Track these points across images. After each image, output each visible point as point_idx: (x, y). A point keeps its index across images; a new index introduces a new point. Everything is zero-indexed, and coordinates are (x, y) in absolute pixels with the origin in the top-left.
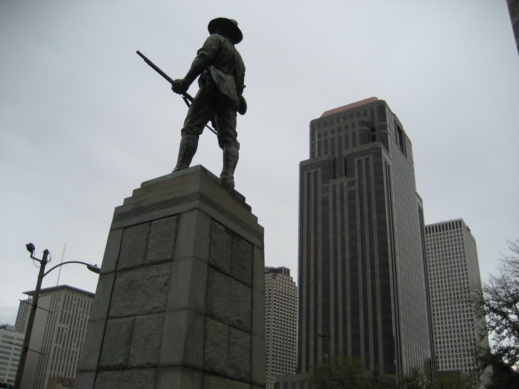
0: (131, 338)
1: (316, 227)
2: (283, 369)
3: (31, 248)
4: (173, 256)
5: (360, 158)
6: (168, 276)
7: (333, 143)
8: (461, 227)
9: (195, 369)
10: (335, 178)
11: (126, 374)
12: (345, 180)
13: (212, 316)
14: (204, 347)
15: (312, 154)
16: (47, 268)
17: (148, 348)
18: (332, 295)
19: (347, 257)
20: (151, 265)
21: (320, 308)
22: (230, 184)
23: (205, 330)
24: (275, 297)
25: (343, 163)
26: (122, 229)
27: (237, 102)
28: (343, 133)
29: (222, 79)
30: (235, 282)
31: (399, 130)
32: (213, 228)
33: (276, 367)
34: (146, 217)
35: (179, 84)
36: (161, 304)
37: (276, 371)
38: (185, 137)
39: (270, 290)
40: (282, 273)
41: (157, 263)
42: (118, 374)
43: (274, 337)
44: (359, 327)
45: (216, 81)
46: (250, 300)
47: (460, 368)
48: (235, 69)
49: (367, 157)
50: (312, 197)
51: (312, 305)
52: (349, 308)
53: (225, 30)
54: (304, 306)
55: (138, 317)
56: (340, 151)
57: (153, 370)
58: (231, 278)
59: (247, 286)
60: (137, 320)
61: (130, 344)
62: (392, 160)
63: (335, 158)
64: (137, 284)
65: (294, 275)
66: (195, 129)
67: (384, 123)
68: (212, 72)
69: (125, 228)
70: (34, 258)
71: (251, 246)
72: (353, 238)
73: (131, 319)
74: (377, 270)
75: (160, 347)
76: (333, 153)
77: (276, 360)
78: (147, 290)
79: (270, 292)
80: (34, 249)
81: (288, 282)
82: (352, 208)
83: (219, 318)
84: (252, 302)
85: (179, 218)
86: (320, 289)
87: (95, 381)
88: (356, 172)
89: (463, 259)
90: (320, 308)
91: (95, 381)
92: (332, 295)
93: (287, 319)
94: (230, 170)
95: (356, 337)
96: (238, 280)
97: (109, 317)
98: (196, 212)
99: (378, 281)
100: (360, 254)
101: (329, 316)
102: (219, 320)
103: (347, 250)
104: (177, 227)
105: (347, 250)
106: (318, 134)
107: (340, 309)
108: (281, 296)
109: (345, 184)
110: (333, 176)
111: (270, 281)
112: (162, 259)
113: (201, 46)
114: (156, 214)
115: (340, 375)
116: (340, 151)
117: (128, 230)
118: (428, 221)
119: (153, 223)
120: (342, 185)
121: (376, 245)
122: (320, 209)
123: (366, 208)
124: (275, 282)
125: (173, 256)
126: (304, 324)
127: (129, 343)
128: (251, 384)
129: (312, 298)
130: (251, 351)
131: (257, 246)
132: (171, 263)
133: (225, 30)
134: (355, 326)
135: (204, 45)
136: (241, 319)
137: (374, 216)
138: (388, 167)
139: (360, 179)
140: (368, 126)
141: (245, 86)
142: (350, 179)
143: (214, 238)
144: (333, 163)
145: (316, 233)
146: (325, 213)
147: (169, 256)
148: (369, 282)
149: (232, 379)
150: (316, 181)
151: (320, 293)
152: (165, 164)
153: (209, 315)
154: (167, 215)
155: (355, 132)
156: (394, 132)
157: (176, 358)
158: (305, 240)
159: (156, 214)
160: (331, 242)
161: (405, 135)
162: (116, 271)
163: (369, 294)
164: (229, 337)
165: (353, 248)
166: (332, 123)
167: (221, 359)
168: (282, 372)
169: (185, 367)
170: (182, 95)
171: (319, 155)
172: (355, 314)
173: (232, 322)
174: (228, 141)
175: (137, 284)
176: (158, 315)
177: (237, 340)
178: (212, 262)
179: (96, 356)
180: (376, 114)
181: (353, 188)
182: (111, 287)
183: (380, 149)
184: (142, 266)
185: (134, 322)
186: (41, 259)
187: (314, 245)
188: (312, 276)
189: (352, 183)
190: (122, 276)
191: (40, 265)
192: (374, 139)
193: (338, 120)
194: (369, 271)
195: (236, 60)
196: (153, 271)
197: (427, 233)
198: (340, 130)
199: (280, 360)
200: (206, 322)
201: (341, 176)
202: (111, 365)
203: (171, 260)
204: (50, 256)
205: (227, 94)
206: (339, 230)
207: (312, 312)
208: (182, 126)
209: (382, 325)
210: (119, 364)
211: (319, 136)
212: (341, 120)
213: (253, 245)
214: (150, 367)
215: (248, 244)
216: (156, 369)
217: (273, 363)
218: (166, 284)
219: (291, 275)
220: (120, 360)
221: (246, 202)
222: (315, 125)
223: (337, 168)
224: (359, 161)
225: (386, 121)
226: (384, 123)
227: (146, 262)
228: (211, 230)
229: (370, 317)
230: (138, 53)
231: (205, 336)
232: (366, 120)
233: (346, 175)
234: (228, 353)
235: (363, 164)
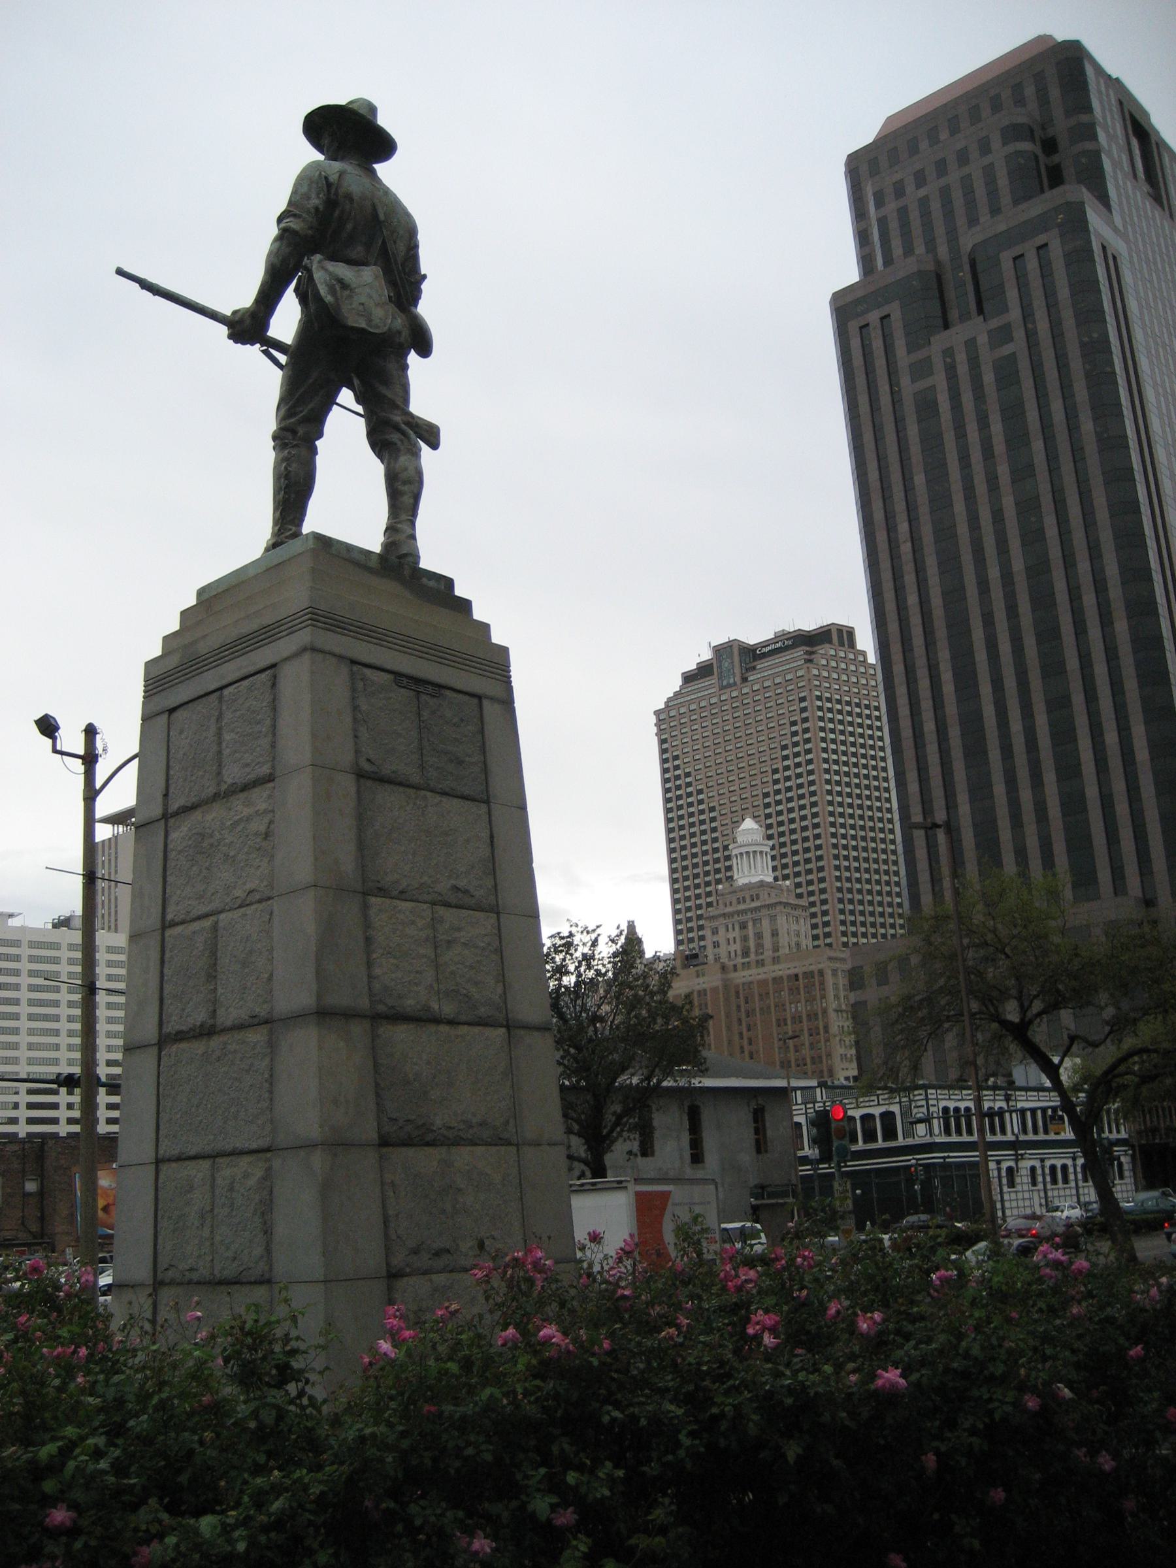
0: (215, 964)
1: (908, 488)
2: (873, 925)
3: (47, 727)
4: (273, 767)
5: (1017, 251)
6: (270, 816)
7: (926, 214)
9: (349, 1015)
10: (946, 326)
11: (215, 1042)
12: (977, 329)
13: (382, 892)
14: (369, 964)
15: (866, 262)
16: (102, 771)
17: (249, 984)
18: (986, 689)
19: (1018, 566)
20: (234, 792)
21: (954, 732)
22: (405, 555)
23: (367, 925)
24: (821, 719)
25: (965, 274)
26: (166, 716)
27: (399, 333)
28: (954, 176)
29: (344, 285)
30: (438, 798)
31: (1140, 130)
32: (360, 685)
33: (853, 923)
34: (210, 680)
35: (241, 321)
36: (262, 881)
37: (855, 935)
38: (281, 456)
39: (803, 699)
40: (830, 642)
41: (245, 788)
42: (198, 1047)
43: (834, 835)
45: (329, 299)
46: (485, 834)
48: (384, 242)
49: (1040, 239)
51: (929, 727)
52: (1041, 720)
53: (348, 133)
54: (907, 732)
55: (222, 916)
56: (952, 236)
57: (264, 1030)
58: (423, 793)
59: (474, 800)
60: (221, 924)
61: (215, 977)
62: (1124, 236)
63: (938, 263)
64: (212, 840)
65: (866, 641)
66: (301, 431)
67: (1084, 118)
68: (318, 275)
69: (172, 711)
70: (62, 753)
71: (475, 701)
72: (1028, 507)
73: (207, 923)
74: (1115, 592)
75: (270, 979)
77: (851, 901)
78: (232, 854)
79: (803, 705)
80: (57, 728)
81: (853, 668)
82: (1013, 413)
83: (402, 892)
84: (492, 837)
85: (275, 677)
86: (947, 676)
87: (159, 1066)
88: (1012, 294)
90: (954, 732)
91: (159, 1066)
92: (986, 689)
93: (866, 777)
94: (404, 517)
95: (1073, 804)
96: (444, 794)
97: (167, 924)
98: (307, 656)
99: (1121, 626)
100: (1055, 553)
102: (403, 895)
103: (1015, 544)
104: (274, 700)
105: (1015, 544)
106: (874, 194)
107: (1016, 726)
108: (840, 712)
109: (983, 339)
110: (940, 322)
111: (800, 673)
112: (252, 777)
113: (282, 206)
114: (231, 670)
115: (994, 931)
116: (952, 236)
117: (179, 715)
119: (226, 692)
120: (971, 344)
121: (1102, 515)
122: (913, 430)
123: (1057, 407)
124: (815, 672)
125: (273, 767)
126: (913, 787)
127: (212, 975)
128: (508, 1027)
129: (926, 705)
130: (500, 951)
131: (491, 699)
132: (271, 785)
133: (348, 133)
134: (1069, 771)
135: (290, 203)
136: (462, 883)
137: (1087, 426)
139: (1027, 315)
140: (1032, 138)
141: (424, 277)
142: (994, 323)
143: (364, 707)
144: (936, 282)
146: (932, 441)
147: (265, 770)
148: (1094, 633)
149: (452, 1022)
150: (888, 349)
151: (948, 689)
152: (240, 533)
153: (370, 888)
154: (252, 669)
156: (1122, 141)
157: (305, 999)
158: (881, 537)
159: (231, 670)
160: (963, 530)
161: (1162, 144)
162: (165, 816)
163: (1100, 670)
164: (434, 929)
165: (1033, 537)
166: (914, 150)
167: (416, 984)
168: (874, 936)
169: (323, 1014)
170: (258, 345)
171: (888, 261)
172: (1063, 735)
173: (440, 894)
174: (399, 437)
175: (212, 840)
176: (261, 906)
177: (457, 934)
178: (367, 767)
179: (153, 1010)
180: (1055, 93)
181: (1007, 350)
182: (161, 855)
183: (1079, 208)
184: (216, 797)
185: (215, 928)
186: (81, 752)
187: (909, 544)
188: (918, 641)
189: (1003, 335)
190: (179, 827)
191: (82, 769)
192: (1056, 178)
193: (933, 136)
194: (1089, 599)
195: (382, 217)
196: (240, 807)
198: (941, 167)
199: (871, 903)
200: (365, 907)
201: (964, 317)
202: (184, 1028)
203: (270, 778)
204: (103, 740)
205: (363, 325)
206: (981, 487)
207: (932, 750)
208: (272, 426)
210: (198, 1024)
211: (879, 204)
212: (944, 135)
213: (480, 698)
214: (259, 1024)
215: (466, 698)
216: (269, 1026)
217: (842, 912)
218: (267, 835)
219: (860, 645)
220: (199, 1016)
221: (458, 592)
222: (863, 169)
223: (951, 294)
224: (1015, 259)
225: (1089, 109)
226: (1084, 118)
227: (224, 787)
228: (354, 690)
229: (1111, 738)
230: (120, 272)
231: (368, 940)
232: (1021, 120)
233: (980, 311)
234: (437, 967)
235: (1032, 264)
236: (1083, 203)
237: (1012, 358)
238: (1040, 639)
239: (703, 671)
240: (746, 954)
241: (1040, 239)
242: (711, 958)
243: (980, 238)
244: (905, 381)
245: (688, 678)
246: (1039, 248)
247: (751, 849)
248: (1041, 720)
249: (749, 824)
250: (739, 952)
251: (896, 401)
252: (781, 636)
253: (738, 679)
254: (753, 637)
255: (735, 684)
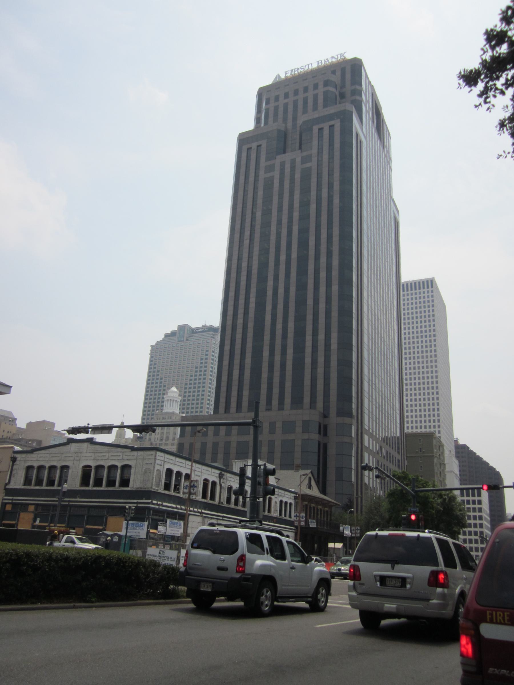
5: (321, 126)
8: (432, 287)
10: (284, 152)
12: (298, 156)
19: (294, 255)
44: (304, 352)
47: (432, 430)
49: (331, 123)
50: (252, 179)
52: (291, 325)
56: (295, 119)
76: (285, 120)
89: (433, 343)
100: (312, 252)
101: (293, 382)
107: (279, 326)
109: (298, 160)
116: (295, 119)
118: (406, 277)
120: (293, 162)
129: (241, 311)
138: (360, 143)
142: (305, 154)
145: (252, 226)
148: (323, 289)
155: (297, 100)
163: (322, 306)
171: (266, 123)
181: (308, 165)
189: (305, 160)
197: (403, 291)
207: (239, 331)
209: (338, 349)
211: (267, 103)
225: (361, 85)
229: (321, 337)
233: (300, 148)
235: (326, 132)
236: (352, 112)
237: (310, 169)
238: (298, 289)
239: (173, 334)
240: (162, 440)
241: (331, 123)
242: (147, 439)
243: (306, 119)
244: (262, 173)
245: (167, 336)
246: (330, 126)
247: (172, 399)
248: (291, 325)
249: (174, 389)
250: (159, 439)
251: (256, 180)
252: (204, 327)
253: (185, 339)
254: (194, 325)
255: (183, 341)
